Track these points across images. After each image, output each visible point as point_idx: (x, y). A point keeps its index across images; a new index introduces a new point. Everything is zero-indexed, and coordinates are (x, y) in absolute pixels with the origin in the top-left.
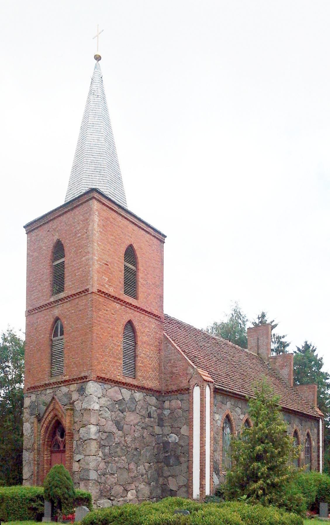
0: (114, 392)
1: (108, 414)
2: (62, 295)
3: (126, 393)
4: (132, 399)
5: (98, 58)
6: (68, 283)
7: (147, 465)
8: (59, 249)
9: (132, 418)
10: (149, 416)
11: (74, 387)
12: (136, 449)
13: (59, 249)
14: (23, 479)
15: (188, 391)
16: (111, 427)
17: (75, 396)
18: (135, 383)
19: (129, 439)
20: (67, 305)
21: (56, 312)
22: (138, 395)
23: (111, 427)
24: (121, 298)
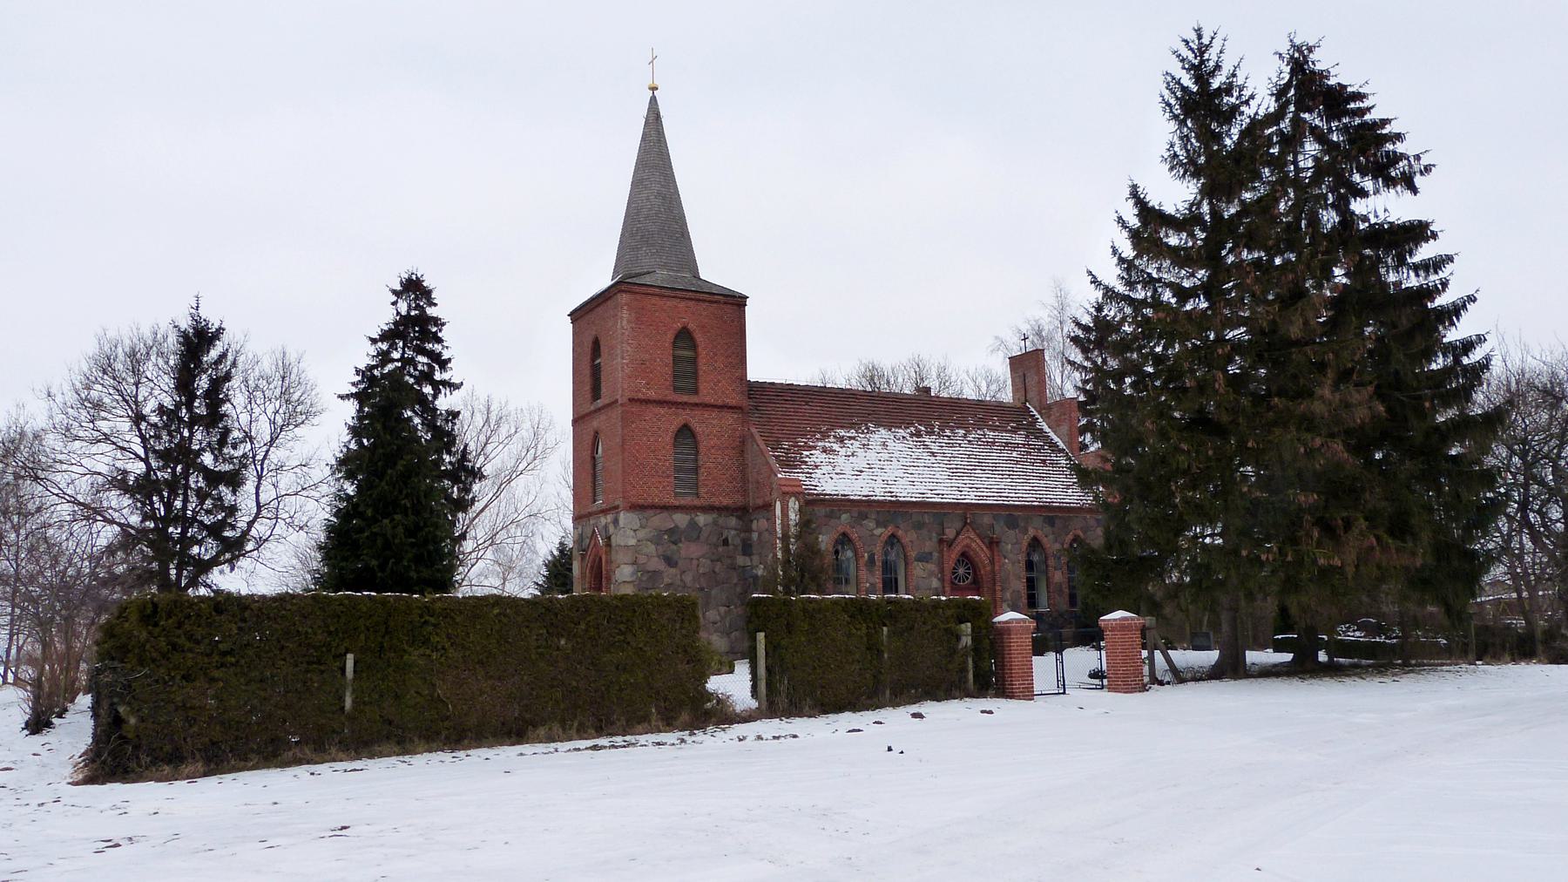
0: (660, 521)
1: (652, 548)
2: (600, 403)
3: (681, 519)
4: (693, 525)
5: (654, 89)
6: (604, 390)
7: (722, 609)
8: (596, 345)
9: (690, 551)
10: (726, 542)
11: (610, 518)
12: (702, 589)
13: (596, 345)
14: (1059, 651)
15: (768, 507)
16: (656, 564)
17: (611, 529)
18: (697, 502)
19: (688, 578)
20: (603, 417)
21: (595, 424)
22: (702, 519)
23: (656, 564)
24: (669, 398)
